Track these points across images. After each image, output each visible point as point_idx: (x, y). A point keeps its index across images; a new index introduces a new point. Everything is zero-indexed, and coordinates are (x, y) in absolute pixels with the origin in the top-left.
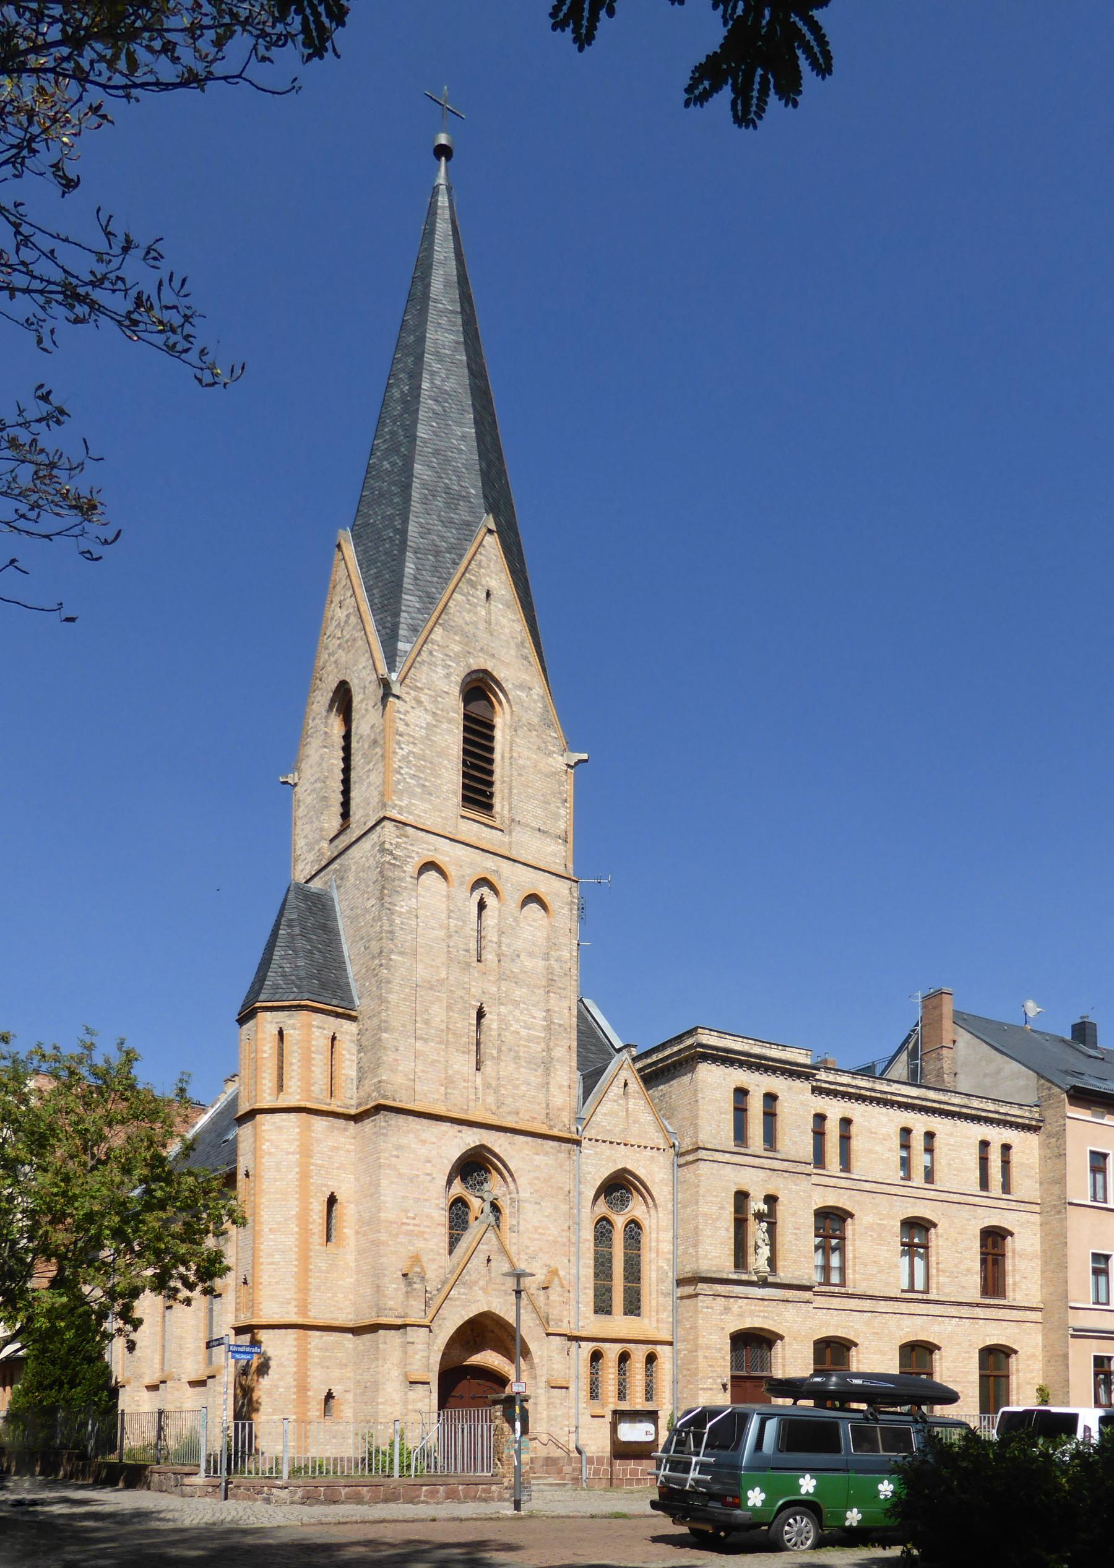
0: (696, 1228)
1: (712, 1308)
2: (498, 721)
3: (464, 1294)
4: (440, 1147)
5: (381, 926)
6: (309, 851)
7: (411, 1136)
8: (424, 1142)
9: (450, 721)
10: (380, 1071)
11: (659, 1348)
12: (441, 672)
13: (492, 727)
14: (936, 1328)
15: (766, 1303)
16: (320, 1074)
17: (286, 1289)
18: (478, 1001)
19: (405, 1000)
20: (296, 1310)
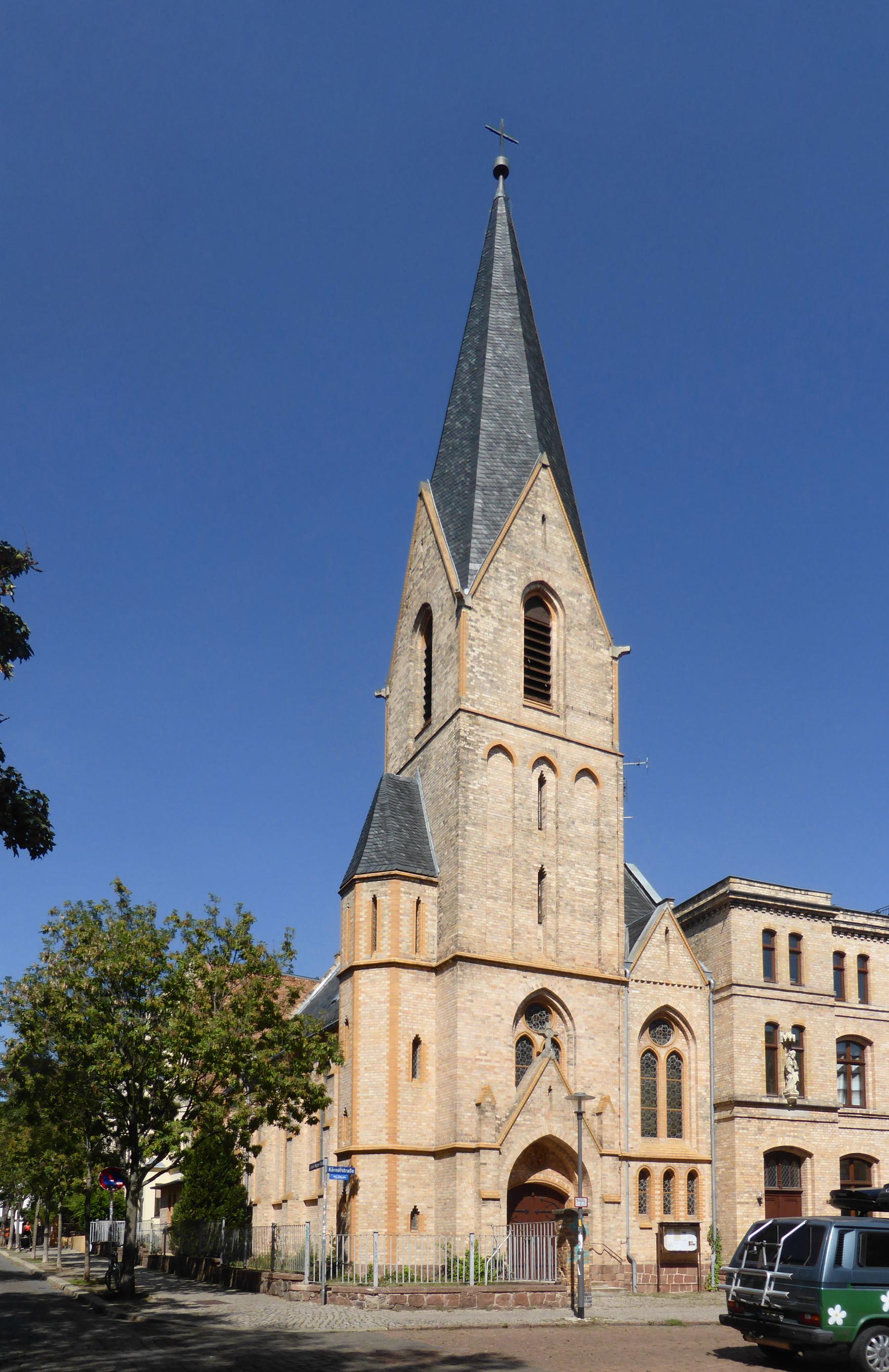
0: (732, 1057)
1: (747, 1129)
3: (530, 1120)
4: (508, 991)
6: (399, 750)
7: (484, 982)
9: (514, 625)
11: (699, 1166)
12: (505, 585)
13: (548, 630)
15: (796, 1123)
16: (406, 931)
19: (477, 864)
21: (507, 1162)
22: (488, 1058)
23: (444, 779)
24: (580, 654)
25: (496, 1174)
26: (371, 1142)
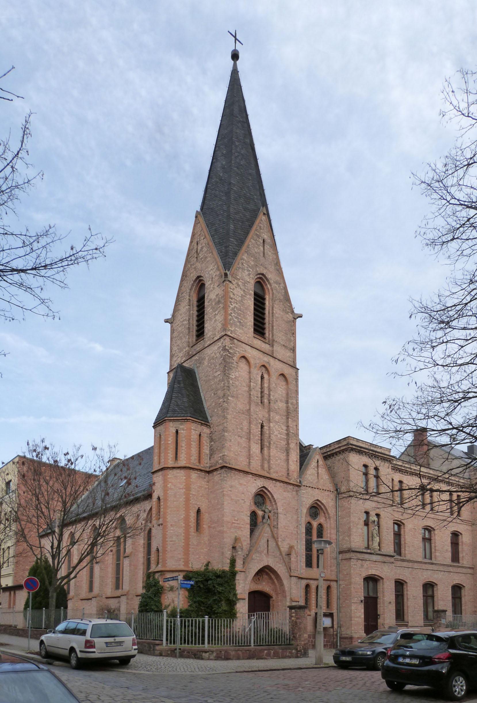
0: (350, 528)
1: (356, 565)
2: (267, 297)
3: (258, 557)
4: (247, 487)
5: (224, 384)
6: (180, 352)
7: (236, 481)
8: (241, 484)
9: (250, 295)
10: (224, 450)
12: (247, 273)
13: (264, 299)
14: (436, 576)
16: (194, 451)
17: (179, 554)
18: (261, 420)
19: (234, 418)
20: (183, 563)
21: (248, 579)
22: (238, 522)
23: (215, 370)
24: (280, 314)
25: (243, 585)
26: (174, 566)
